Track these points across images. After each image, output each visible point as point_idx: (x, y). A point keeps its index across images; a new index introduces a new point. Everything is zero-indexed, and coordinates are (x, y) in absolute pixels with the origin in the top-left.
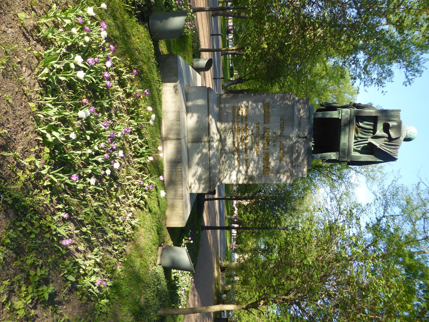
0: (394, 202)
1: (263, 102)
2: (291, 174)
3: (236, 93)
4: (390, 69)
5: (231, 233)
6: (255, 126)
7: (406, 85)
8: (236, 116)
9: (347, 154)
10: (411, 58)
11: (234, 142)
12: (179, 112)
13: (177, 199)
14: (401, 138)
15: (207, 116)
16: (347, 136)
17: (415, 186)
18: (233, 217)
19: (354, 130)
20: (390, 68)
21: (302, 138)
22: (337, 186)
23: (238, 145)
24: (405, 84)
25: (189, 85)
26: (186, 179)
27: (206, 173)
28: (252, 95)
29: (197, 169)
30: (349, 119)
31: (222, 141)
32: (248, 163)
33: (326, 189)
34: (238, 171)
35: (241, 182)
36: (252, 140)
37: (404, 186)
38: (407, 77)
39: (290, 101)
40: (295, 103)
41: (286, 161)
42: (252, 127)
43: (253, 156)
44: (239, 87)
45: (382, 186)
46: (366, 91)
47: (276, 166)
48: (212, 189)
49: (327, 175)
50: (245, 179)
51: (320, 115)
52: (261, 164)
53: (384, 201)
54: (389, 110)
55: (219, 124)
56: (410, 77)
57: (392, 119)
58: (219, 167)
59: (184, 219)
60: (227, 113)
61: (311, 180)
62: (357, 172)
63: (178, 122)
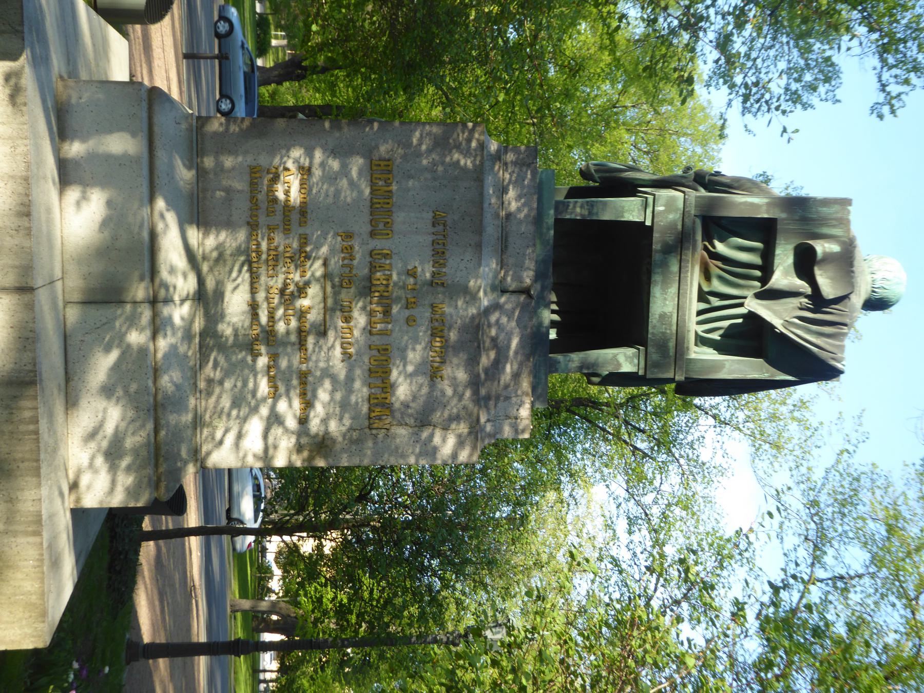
0: (847, 528)
1: (368, 153)
2: (471, 427)
3: (269, 115)
4: (828, 59)
5: (255, 670)
6: (338, 247)
7: (881, 117)
8: (264, 206)
9: (672, 352)
10: (897, 21)
11: (254, 307)
12: (26, 179)
13: (15, 534)
14: (853, 296)
15: (146, 199)
16: (673, 290)
17: (913, 472)
18: (264, 606)
19: (697, 269)
20: (828, 53)
21: (513, 292)
22: (650, 475)
23: (271, 317)
24: (876, 110)
25: (73, 73)
26: (55, 450)
27: (143, 426)
28: (327, 125)
29: (105, 411)
30: (680, 227)
31: (207, 299)
32: (309, 388)
33: (614, 486)
34: (269, 418)
35: (280, 462)
36: (325, 299)
37: (878, 471)
38: (883, 87)
39: (467, 153)
40: (487, 163)
41: (454, 383)
42: (324, 250)
43: (328, 360)
44: (288, 94)
45: (803, 470)
46: (748, 130)
47: (414, 398)
48: (162, 490)
49: (617, 436)
50: (299, 448)
51: (578, 210)
52: (361, 391)
53: (813, 526)
54: (814, 200)
55: (194, 235)
56: (894, 89)
57: (825, 230)
58: (192, 402)
59: (44, 614)
60: (228, 190)
61: (560, 457)
62: (721, 422)
63: (25, 222)
